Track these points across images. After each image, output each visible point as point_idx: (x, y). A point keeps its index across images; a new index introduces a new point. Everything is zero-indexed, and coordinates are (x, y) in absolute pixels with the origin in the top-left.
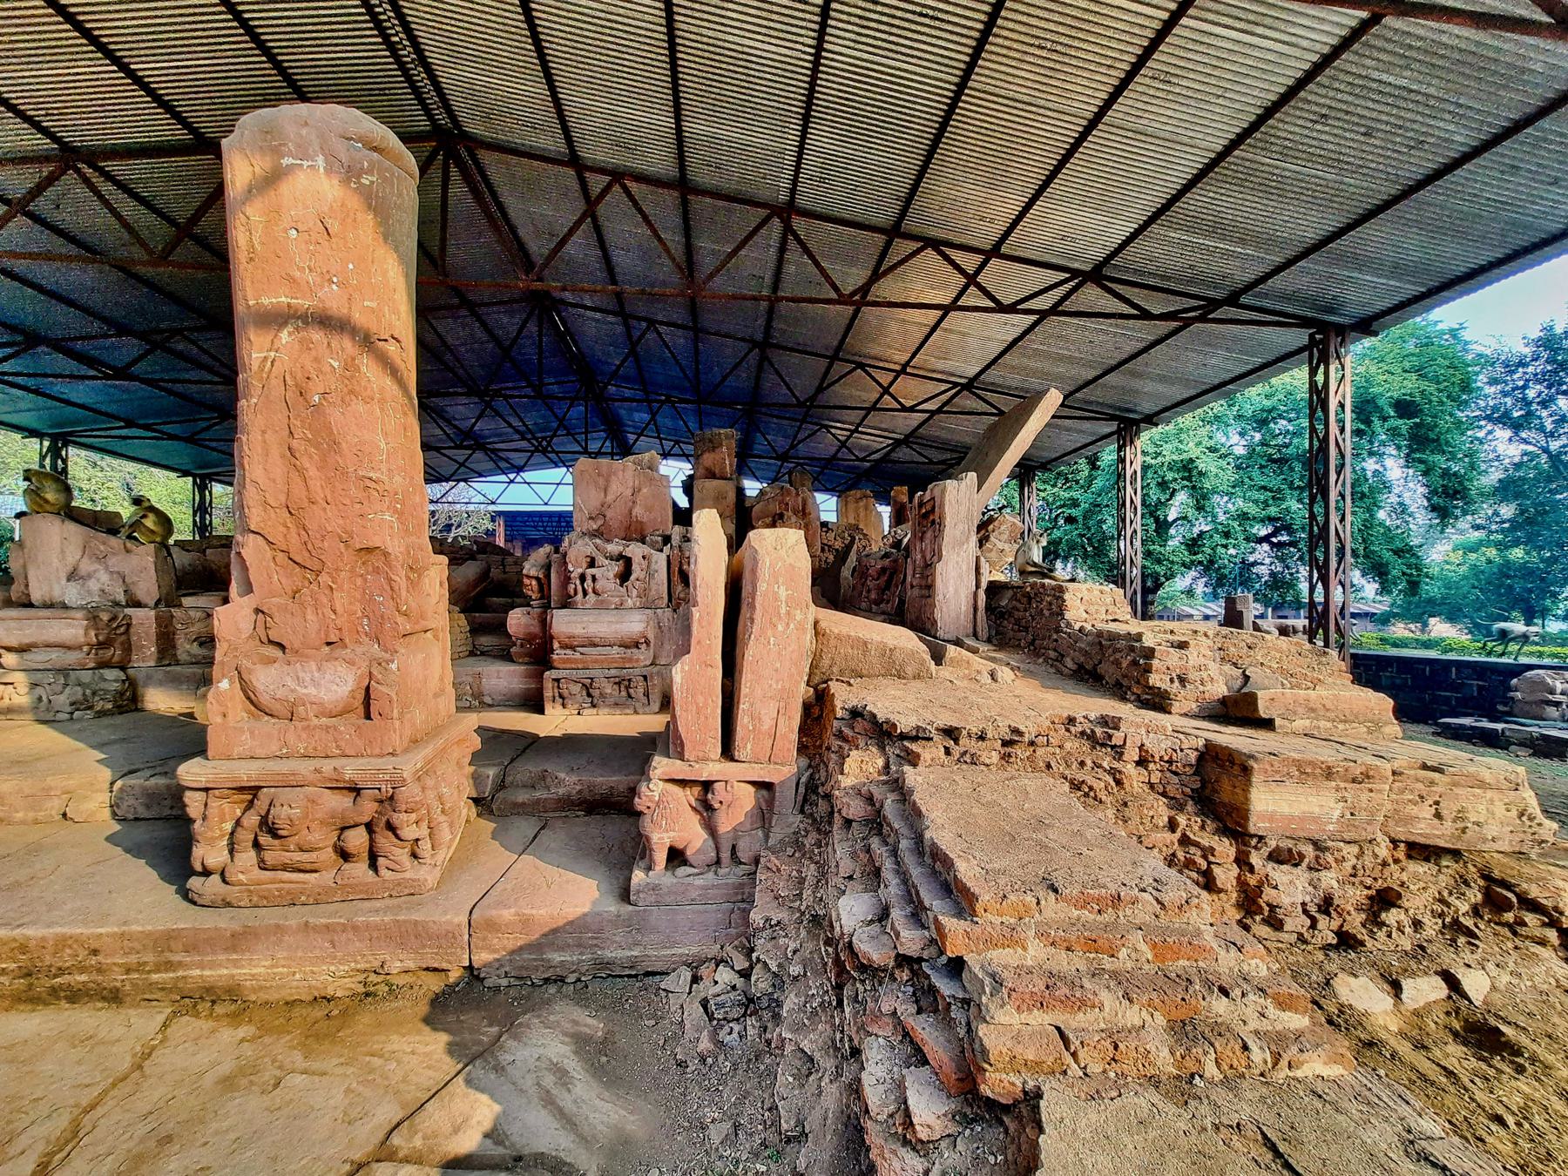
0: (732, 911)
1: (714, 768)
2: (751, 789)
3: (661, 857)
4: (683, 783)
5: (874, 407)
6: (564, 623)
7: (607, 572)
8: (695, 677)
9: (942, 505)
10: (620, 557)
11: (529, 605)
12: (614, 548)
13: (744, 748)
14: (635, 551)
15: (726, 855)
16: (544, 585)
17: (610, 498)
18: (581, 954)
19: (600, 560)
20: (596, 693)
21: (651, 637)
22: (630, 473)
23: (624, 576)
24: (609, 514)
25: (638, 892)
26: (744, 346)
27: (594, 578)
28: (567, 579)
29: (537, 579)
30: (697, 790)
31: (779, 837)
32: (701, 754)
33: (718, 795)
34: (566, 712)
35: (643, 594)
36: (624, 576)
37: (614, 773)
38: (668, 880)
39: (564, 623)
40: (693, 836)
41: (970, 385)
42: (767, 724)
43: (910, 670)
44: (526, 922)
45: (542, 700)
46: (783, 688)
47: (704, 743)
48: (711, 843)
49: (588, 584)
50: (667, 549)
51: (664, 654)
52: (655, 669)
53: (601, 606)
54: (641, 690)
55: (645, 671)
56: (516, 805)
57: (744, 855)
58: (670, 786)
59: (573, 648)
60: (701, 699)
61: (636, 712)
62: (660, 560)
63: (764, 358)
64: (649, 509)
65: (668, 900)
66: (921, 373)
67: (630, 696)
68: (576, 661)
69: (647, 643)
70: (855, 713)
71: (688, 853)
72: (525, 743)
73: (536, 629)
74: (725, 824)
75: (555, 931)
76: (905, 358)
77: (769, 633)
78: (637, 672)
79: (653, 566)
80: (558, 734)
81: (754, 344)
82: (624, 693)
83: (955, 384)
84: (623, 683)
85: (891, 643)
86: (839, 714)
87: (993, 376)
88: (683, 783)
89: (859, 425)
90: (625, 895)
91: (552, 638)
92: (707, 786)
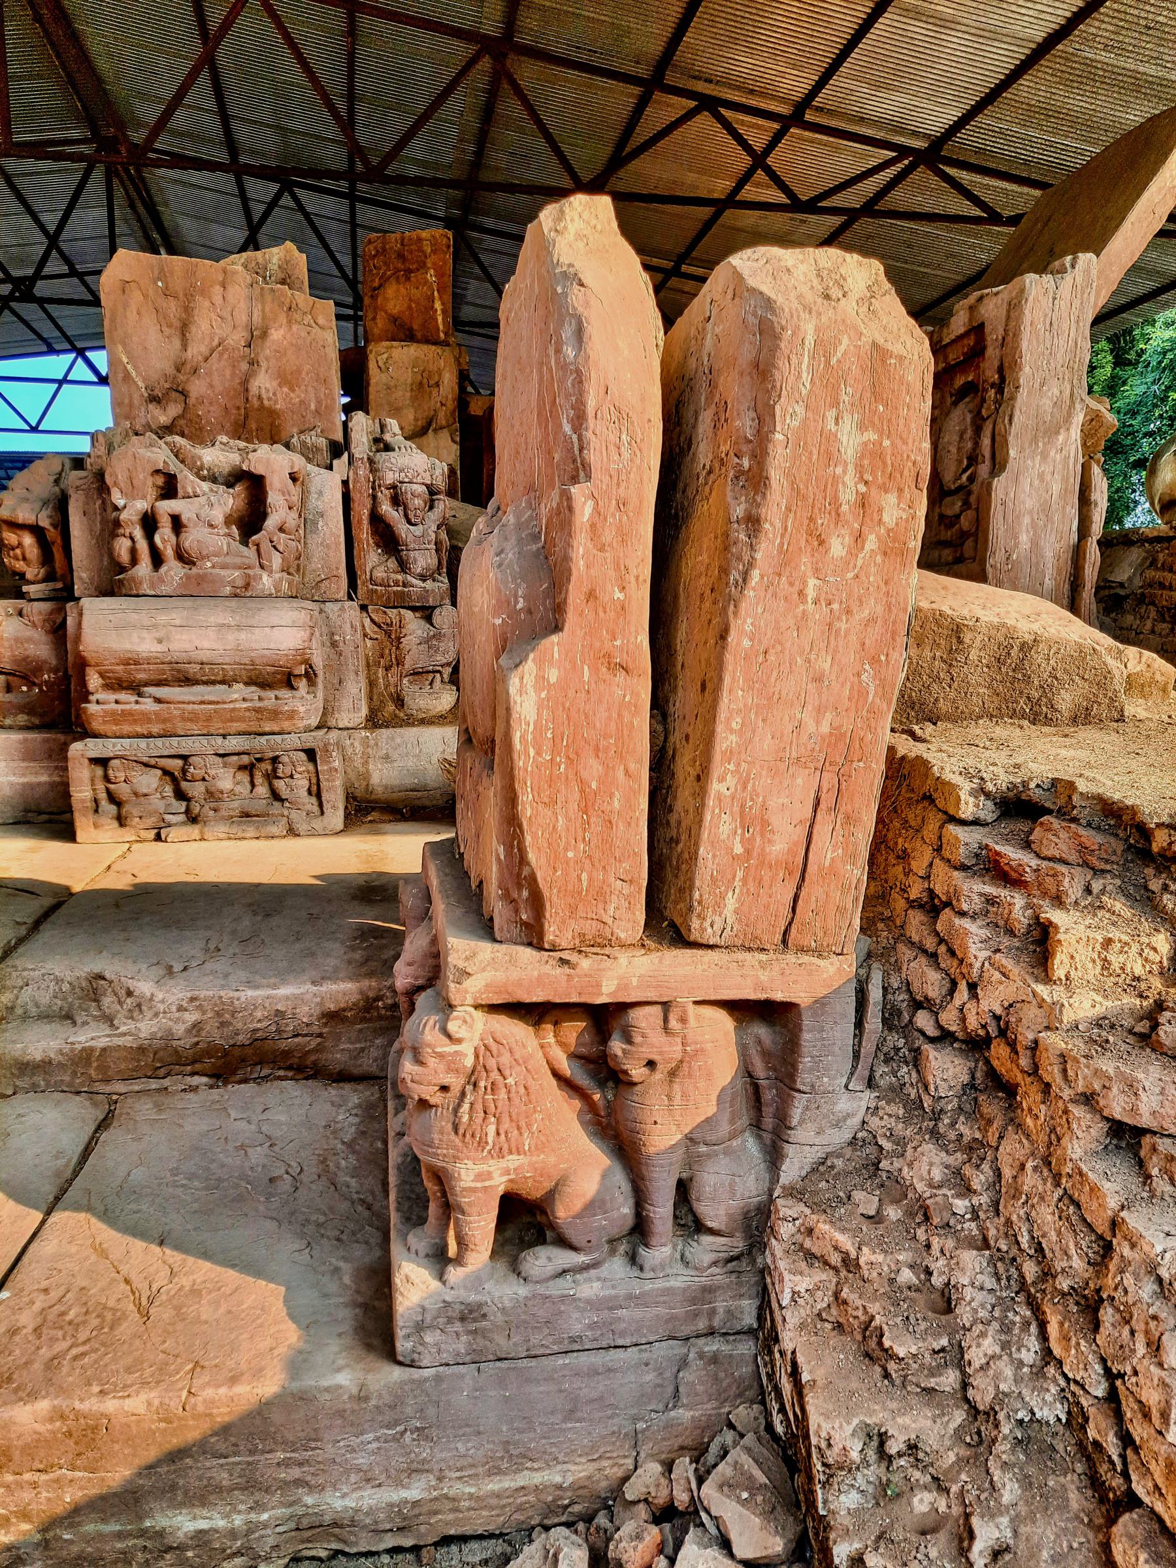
0: (683, 1363)
1: (628, 971)
2: (724, 1021)
3: (481, 1225)
4: (534, 1013)
5: (731, 201)
6: (109, 629)
7: (208, 509)
8: (574, 700)
9: (1010, 339)
10: (237, 477)
11: (20, 595)
12: (219, 455)
13: (722, 898)
14: (271, 461)
15: (662, 1210)
16: (53, 546)
17: (196, 350)
18: (258, 1507)
19: (187, 480)
20: (196, 790)
21: (318, 661)
22: (238, 293)
23: (250, 521)
24: (197, 388)
25: (420, 1328)
26: (461, 50)
27: (177, 524)
28: (112, 527)
29: (36, 531)
30: (574, 1030)
31: (811, 1156)
32: (590, 928)
33: (645, 1043)
34: (128, 835)
35: (295, 566)
36: (250, 521)
37: (283, 976)
38: (505, 1292)
39: (109, 629)
40: (585, 1175)
41: (934, 154)
42: (783, 840)
43: (1066, 701)
44: (86, 1438)
45: (69, 810)
46: (837, 735)
47: (601, 896)
48: (620, 1179)
49: (164, 536)
50: (341, 464)
51: (346, 703)
52: (333, 735)
53: (198, 591)
54: (302, 783)
55: (309, 740)
56: (25, 1068)
57: (716, 1208)
58: (515, 1030)
59: (136, 688)
60: (592, 769)
61: (292, 832)
62: (327, 487)
63: (501, 77)
64: (287, 379)
65: (502, 1343)
66: (833, 123)
67: (276, 796)
68: (145, 718)
69: (310, 676)
70: (1019, 808)
71: (563, 1213)
72: (30, 909)
73: (40, 648)
74: (663, 1133)
75: (175, 1456)
76: (797, 83)
77: (805, 563)
78: (293, 740)
79: (313, 502)
80: (120, 883)
81: (485, 44)
82: (262, 790)
83: (903, 151)
84: (261, 767)
85: (1025, 629)
86: (968, 807)
87: (996, 132)
88: (534, 1013)
89: (682, 258)
90: (377, 1330)
91: (82, 664)
92: (605, 1018)
